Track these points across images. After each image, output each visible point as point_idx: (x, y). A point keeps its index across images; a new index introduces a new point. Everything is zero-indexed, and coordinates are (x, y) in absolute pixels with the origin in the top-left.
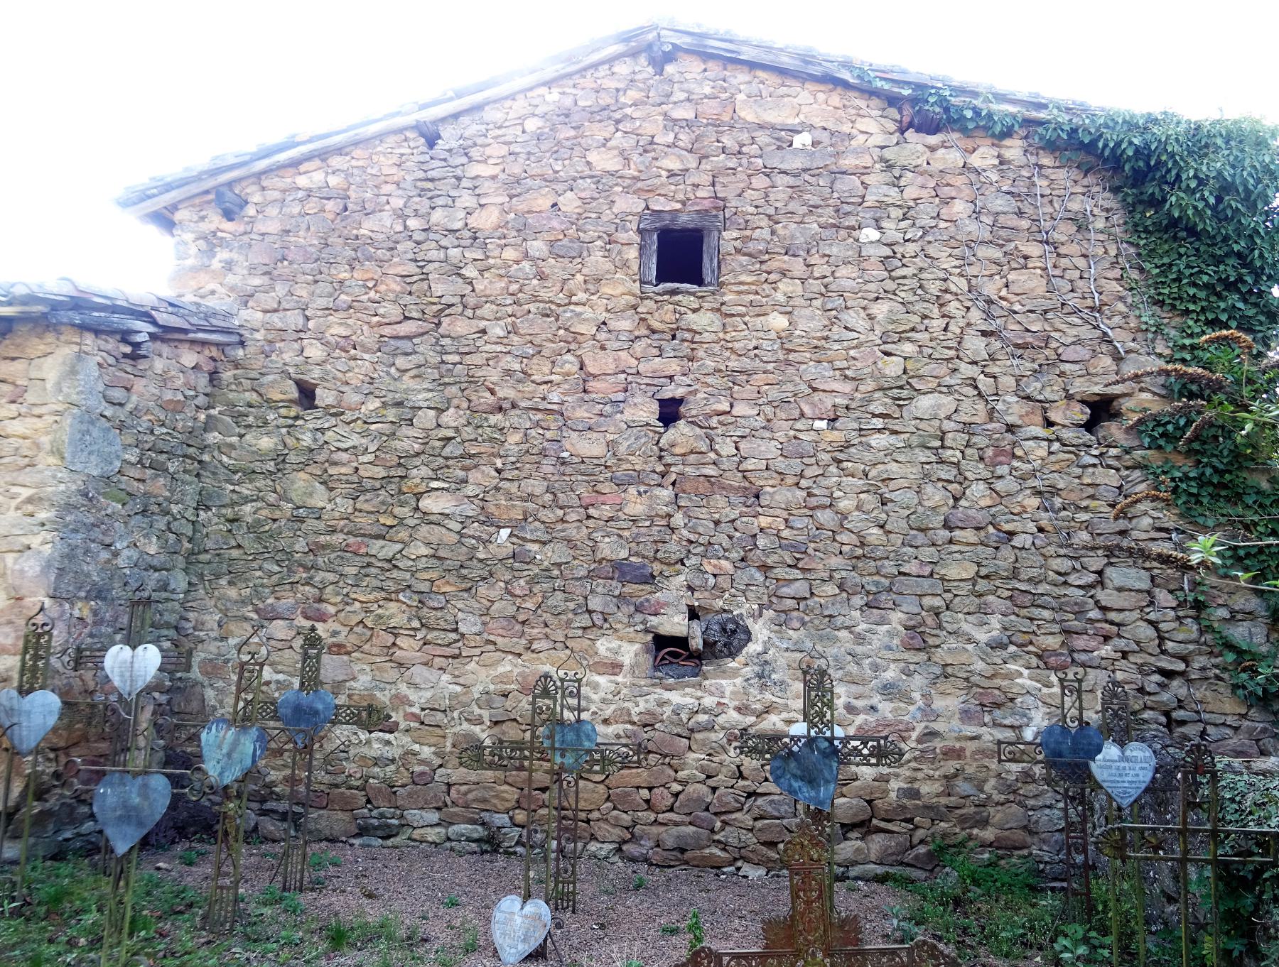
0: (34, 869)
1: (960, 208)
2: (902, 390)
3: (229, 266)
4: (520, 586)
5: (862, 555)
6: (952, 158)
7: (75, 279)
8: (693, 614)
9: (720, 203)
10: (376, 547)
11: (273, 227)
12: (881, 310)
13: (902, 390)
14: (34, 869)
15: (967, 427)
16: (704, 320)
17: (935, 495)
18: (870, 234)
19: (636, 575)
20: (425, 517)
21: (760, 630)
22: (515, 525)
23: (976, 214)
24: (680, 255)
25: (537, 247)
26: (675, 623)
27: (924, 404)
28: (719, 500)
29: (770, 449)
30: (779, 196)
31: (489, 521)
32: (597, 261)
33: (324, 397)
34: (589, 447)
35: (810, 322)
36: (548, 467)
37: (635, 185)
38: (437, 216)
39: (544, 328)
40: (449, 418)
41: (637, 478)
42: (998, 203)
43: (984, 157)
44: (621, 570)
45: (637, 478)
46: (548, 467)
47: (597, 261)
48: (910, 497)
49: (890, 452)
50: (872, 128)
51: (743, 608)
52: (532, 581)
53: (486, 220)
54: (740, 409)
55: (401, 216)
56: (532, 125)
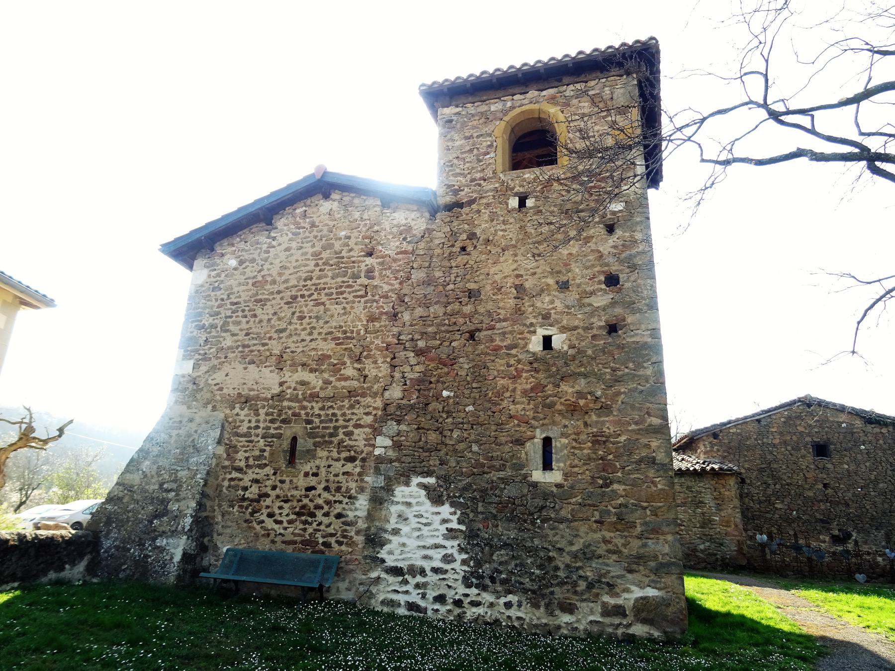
0: (280, 508)
1: (881, 442)
2: (876, 482)
3: (718, 450)
4: (800, 524)
5: (873, 518)
6: (878, 430)
7: (33, 410)
8: (839, 530)
9: (829, 439)
10: (767, 515)
11: (726, 441)
12: (868, 464)
13: (876, 482)
14: (280, 508)
15: (890, 491)
16: (829, 466)
17: (886, 506)
18: (863, 447)
19: (826, 522)
20: (776, 509)
21: (854, 534)
22: (797, 511)
23: (885, 443)
24: (821, 450)
25: (789, 448)
26: (836, 532)
27: (881, 485)
28: (840, 506)
29: (850, 495)
30: (841, 437)
31: (789, 509)
32: (803, 452)
33: (748, 481)
34: (811, 494)
35: (853, 467)
36: (802, 498)
37: (809, 435)
38: (765, 440)
39: (794, 467)
40: (778, 486)
41: (821, 501)
42: (889, 441)
43: (884, 430)
44: (822, 521)
45: (821, 501)
46: (802, 498)
47: (803, 452)
48: (881, 506)
49: (875, 496)
50: (858, 423)
51: (850, 529)
52: (803, 523)
53: (777, 441)
54: (842, 486)
55: (756, 439)
56: (782, 420)
